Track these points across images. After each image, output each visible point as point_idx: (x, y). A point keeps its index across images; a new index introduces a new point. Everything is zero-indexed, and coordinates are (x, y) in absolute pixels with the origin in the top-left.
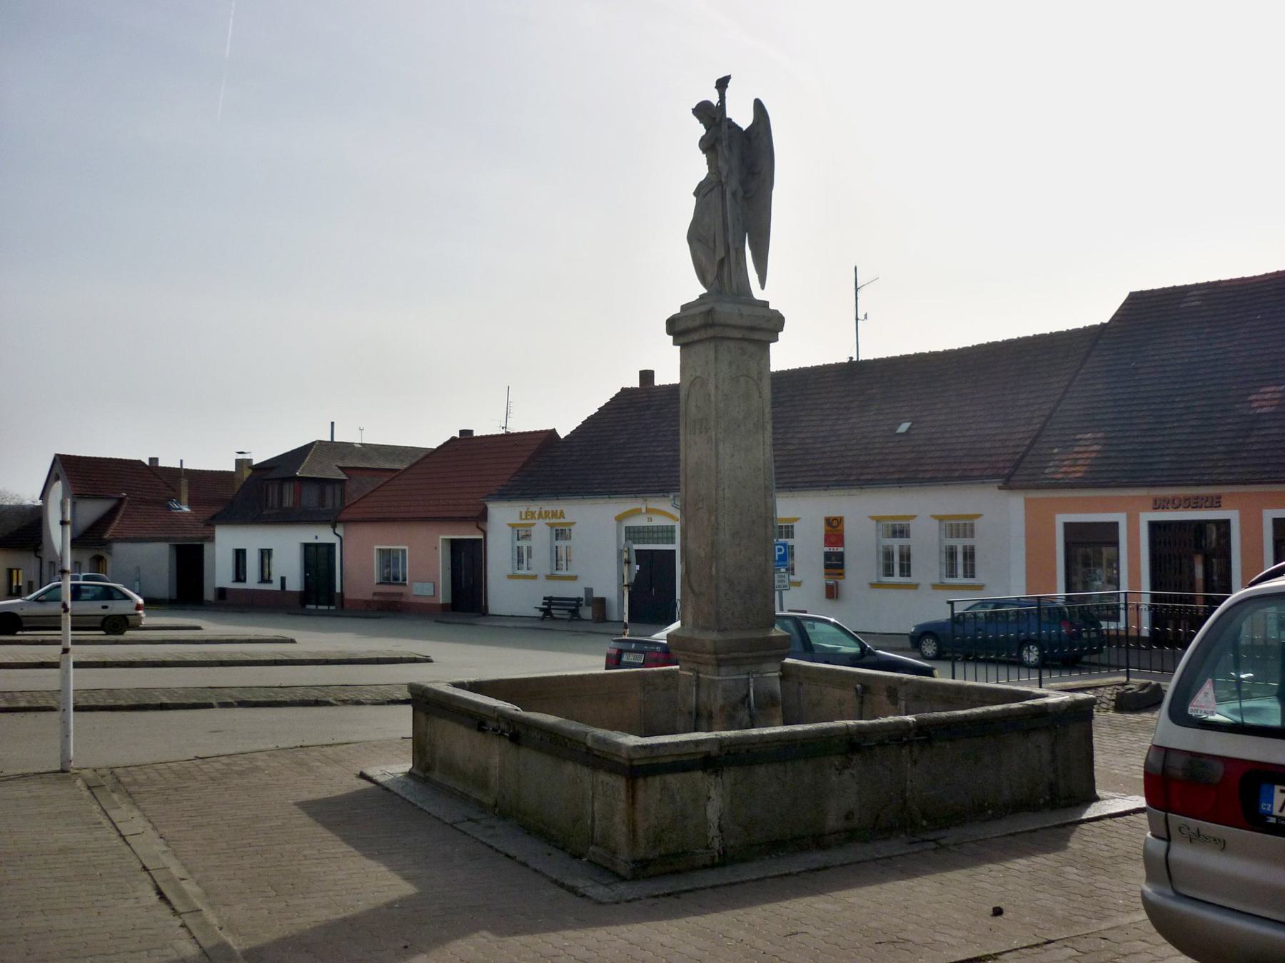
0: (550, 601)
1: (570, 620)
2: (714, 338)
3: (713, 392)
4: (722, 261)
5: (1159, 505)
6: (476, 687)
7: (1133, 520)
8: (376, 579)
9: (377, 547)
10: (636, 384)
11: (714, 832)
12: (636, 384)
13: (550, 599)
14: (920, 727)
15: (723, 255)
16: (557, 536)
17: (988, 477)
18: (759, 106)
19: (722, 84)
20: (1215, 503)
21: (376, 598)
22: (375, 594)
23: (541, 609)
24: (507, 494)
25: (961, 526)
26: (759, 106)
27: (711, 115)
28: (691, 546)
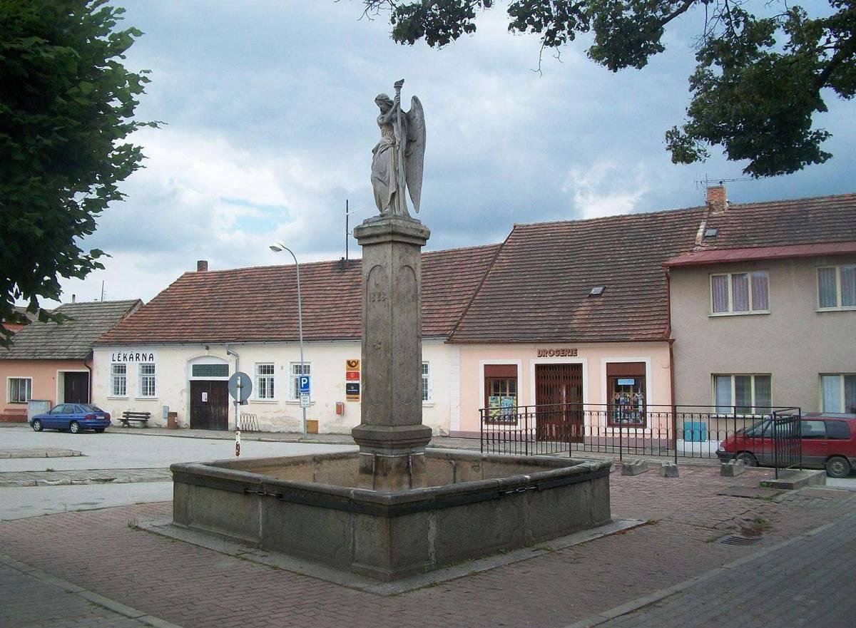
0: (128, 414)
1: (123, 427)
2: (393, 242)
3: (390, 275)
4: (393, 195)
5: (541, 354)
6: (214, 465)
7: (526, 363)
8: (8, 400)
9: (8, 377)
10: (195, 269)
11: (431, 549)
12: (195, 269)
13: (128, 413)
14: (534, 482)
15: (394, 190)
16: (297, 366)
17: (438, 336)
18: (415, 99)
19: (399, 85)
20: (574, 353)
21: (7, 413)
22: (6, 410)
23: (122, 420)
24: (107, 343)
25: (302, 370)
26: (415, 99)
27: (385, 104)
28: (370, 371)
